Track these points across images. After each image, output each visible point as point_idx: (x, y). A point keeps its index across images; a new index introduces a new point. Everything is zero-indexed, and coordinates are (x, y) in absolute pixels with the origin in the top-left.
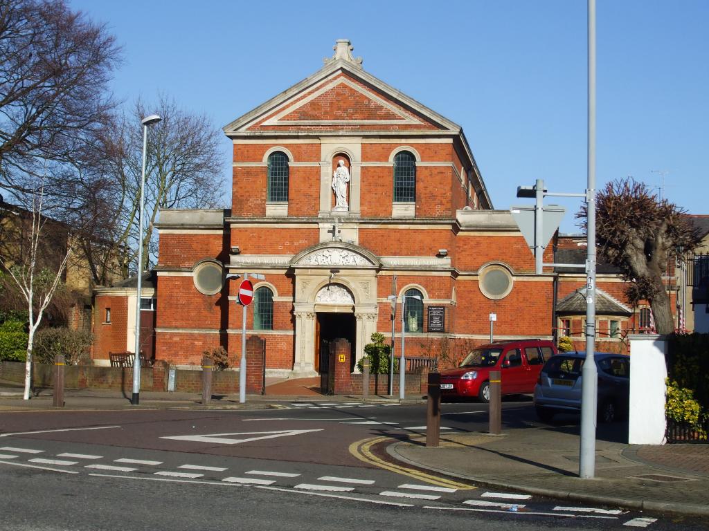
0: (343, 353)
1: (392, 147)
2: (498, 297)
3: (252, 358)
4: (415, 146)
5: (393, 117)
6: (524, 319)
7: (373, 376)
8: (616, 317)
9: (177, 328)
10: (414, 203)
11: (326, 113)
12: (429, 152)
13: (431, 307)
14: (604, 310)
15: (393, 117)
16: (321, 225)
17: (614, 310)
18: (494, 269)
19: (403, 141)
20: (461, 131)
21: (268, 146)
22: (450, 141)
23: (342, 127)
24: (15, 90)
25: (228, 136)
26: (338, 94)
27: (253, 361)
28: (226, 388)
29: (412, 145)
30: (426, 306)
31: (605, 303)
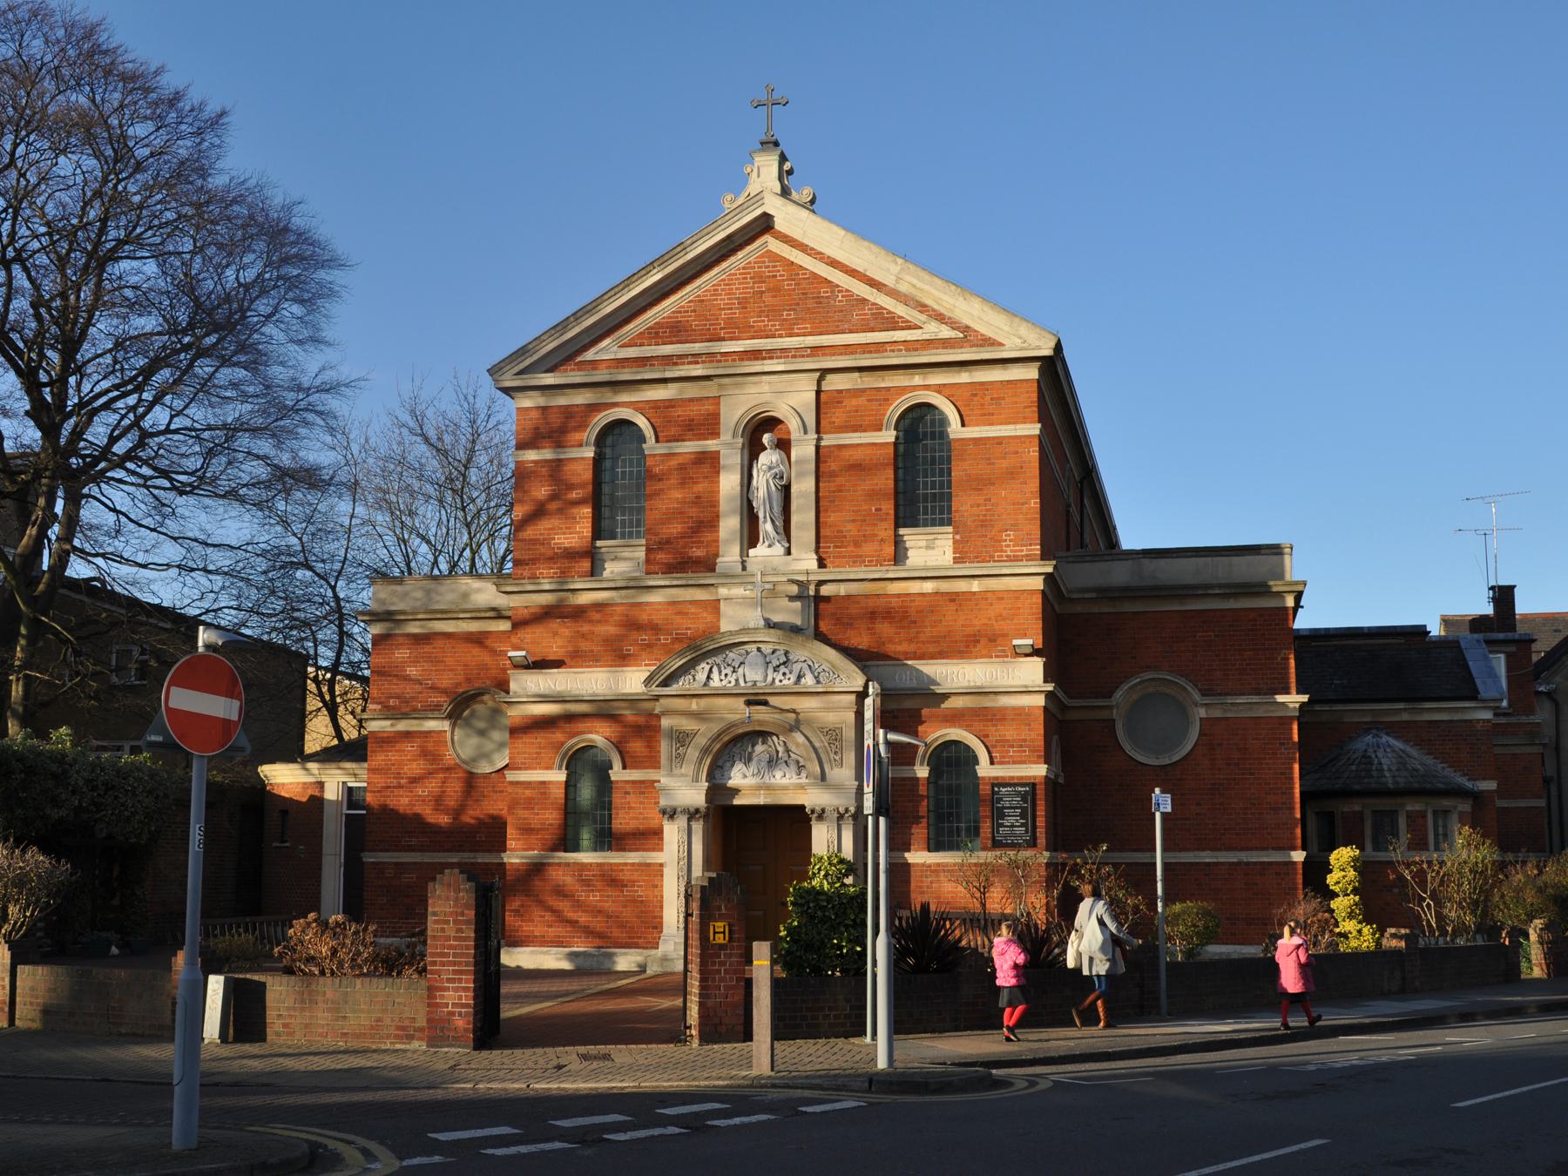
0: (721, 918)
1: (886, 395)
2: (1165, 761)
3: (448, 938)
4: (947, 391)
5: (893, 323)
6: (1390, 770)
7: (1029, 650)
8: (1446, 803)
9: (410, 849)
10: (950, 529)
11: (730, 323)
12: (973, 403)
13: (999, 785)
14: (1416, 785)
15: (893, 323)
16: (723, 591)
17: (1441, 786)
18: (1151, 690)
19: (917, 380)
20: (1058, 348)
21: (594, 408)
22: (1032, 373)
23: (770, 354)
24: (986, 939)
25: (502, 389)
26: (759, 278)
27: (451, 947)
28: (372, 1027)
29: (939, 389)
30: (985, 790)
31: (1417, 770)
